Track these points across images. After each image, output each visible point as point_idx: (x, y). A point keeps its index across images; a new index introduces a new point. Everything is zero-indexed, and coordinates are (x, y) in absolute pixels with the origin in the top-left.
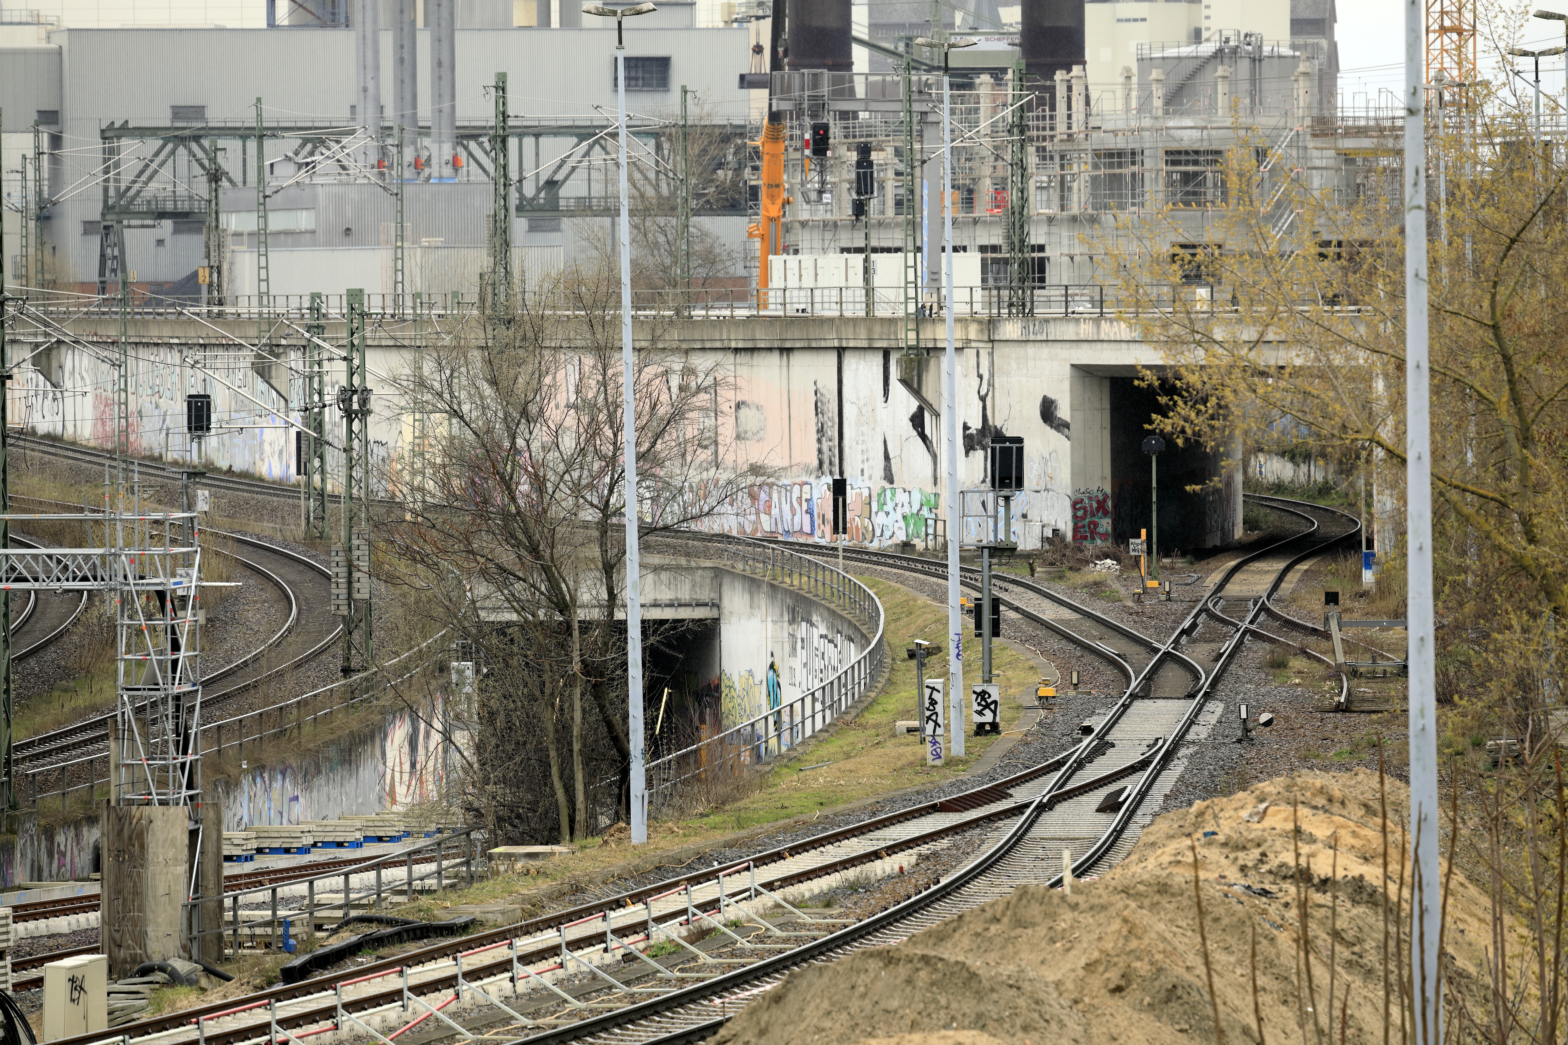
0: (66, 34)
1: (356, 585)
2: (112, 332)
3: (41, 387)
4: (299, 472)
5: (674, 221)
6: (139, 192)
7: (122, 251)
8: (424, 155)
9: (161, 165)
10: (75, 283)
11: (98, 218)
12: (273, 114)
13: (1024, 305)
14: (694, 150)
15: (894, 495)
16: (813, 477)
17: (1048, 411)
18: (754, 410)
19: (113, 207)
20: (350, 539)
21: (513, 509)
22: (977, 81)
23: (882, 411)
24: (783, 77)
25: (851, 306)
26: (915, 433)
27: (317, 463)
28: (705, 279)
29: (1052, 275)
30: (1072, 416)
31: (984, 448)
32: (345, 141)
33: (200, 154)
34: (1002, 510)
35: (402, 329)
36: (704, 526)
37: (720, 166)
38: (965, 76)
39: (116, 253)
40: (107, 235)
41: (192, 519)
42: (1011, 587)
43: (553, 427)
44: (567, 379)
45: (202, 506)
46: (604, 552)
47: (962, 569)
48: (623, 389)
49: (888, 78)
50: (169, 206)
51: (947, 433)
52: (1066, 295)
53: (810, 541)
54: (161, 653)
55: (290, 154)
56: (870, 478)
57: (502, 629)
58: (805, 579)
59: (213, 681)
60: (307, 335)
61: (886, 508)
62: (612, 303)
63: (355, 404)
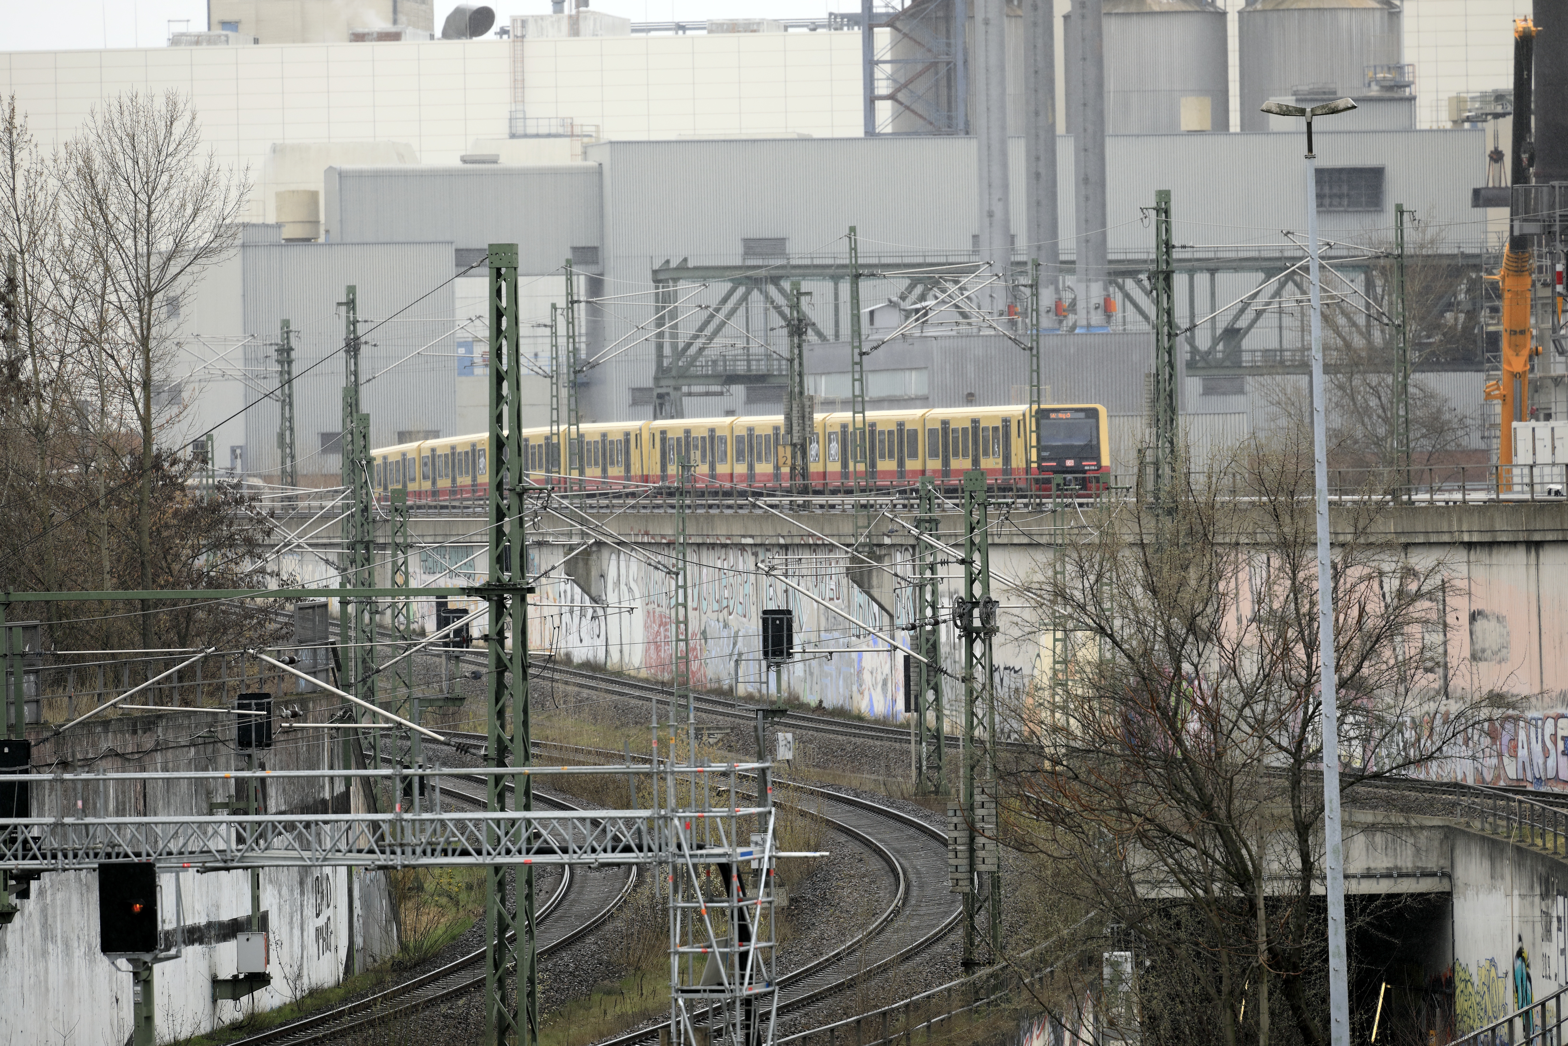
1: (981, 854)
3: (577, 602)
4: (908, 709)
5: (1390, 380)
6: (701, 350)
8: (1067, 297)
11: (650, 383)
14: (1414, 286)
18: (1493, 623)
19: (669, 369)
20: (971, 795)
21: (1179, 755)
24: (1527, 193)
27: (930, 695)
28: (1431, 454)
32: (964, 281)
33: (780, 300)
36: (1433, 772)
37: (1449, 307)
41: (763, 771)
43: (1228, 647)
45: (784, 753)
46: (1297, 808)
48: (1318, 597)
50: (741, 368)
54: (726, 944)
55: (895, 299)
57: (1165, 908)
59: (795, 980)
60: (915, 531)
62: (1301, 487)
63: (977, 619)
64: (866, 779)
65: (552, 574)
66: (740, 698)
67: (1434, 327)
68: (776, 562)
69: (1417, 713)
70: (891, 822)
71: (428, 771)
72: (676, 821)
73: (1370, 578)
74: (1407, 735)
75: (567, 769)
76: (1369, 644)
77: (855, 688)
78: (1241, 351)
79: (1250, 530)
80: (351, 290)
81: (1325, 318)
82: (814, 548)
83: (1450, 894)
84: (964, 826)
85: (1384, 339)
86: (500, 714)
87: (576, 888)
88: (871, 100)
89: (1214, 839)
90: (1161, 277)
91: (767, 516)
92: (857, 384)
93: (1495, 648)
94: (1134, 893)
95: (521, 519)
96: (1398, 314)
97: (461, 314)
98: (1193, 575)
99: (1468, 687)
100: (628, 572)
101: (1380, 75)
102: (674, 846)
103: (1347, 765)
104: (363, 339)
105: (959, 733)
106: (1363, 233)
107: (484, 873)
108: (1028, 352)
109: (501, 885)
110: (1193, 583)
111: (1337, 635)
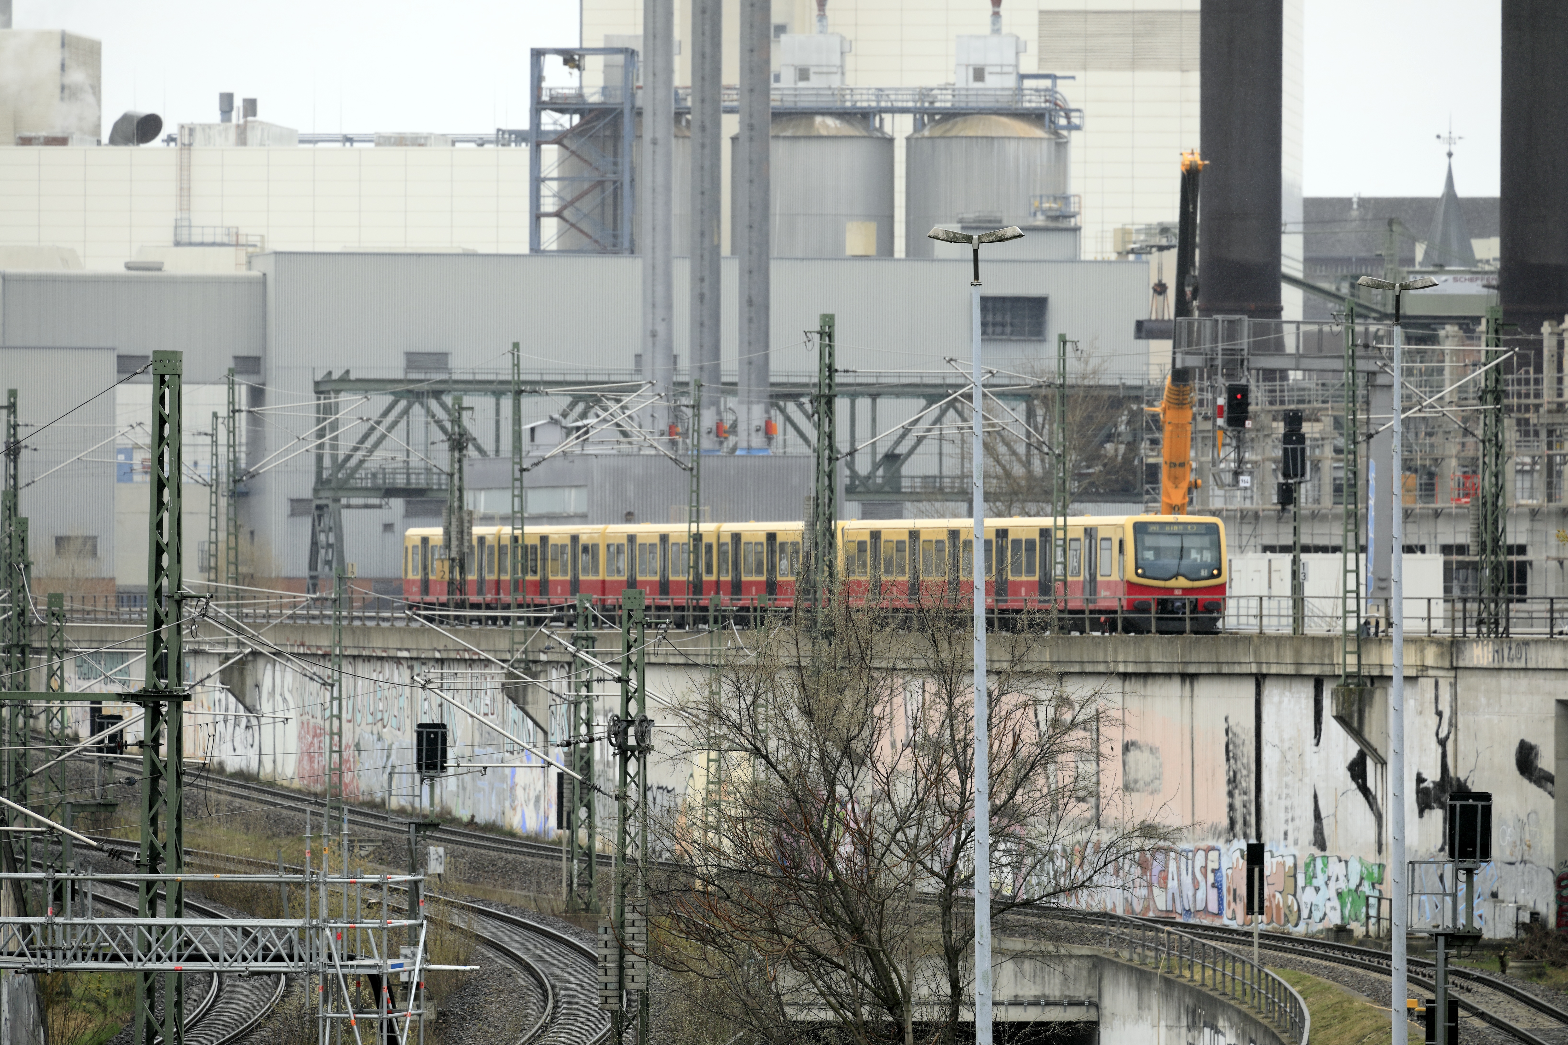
0: (272, 259)
1: (630, 972)
2: (324, 642)
3: (232, 711)
4: (560, 826)
6: (361, 462)
7: (340, 538)
8: (728, 419)
9: (390, 428)
10: (277, 578)
11: (308, 494)
12: (534, 365)
13: (1497, 623)
14: (1077, 416)
15: (1326, 865)
16: (1222, 841)
17: (1526, 759)
19: (328, 481)
20: (622, 913)
21: (831, 878)
22: (1442, 333)
23: (1313, 758)
24: (1190, 325)
25: (1274, 621)
26: (1354, 786)
27: (583, 813)
29: (1535, 585)
30: (1557, 767)
31: (1442, 806)
32: (626, 400)
33: (441, 414)
34: (1462, 886)
35: (696, 643)
36: (1083, 901)
37: (1109, 438)
38: (1427, 326)
39: (332, 540)
40: (320, 516)
41: (416, 883)
42: (1475, 986)
43: (882, 770)
44: (903, 711)
45: (436, 867)
47: (1409, 962)
48: (973, 724)
49: (1326, 328)
50: (400, 481)
51: (1397, 787)
52: (1552, 611)
53: (1217, 923)
55: (556, 416)
56: (1296, 843)
58: (1209, 973)
60: (572, 649)
61: (1316, 882)
63: (632, 738)
64: (517, 895)
65: (207, 683)
66: (393, 811)
67: (1092, 459)
68: (431, 676)
69: (1069, 841)
70: (541, 939)
71: (81, 876)
72: (328, 931)
73: (1026, 705)
74: (1058, 863)
75: (219, 877)
76: (1023, 772)
77: (507, 804)
78: (900, 477)
79: (907, 655)
80: (13, 393)
81: (985, 445)
82: (470, 662)
83: (1097, 1023)
84: (615, 944)
85: (1044, 468)
86: (154, 821)
87: (223, 997)
88: (537, 216)
89: (865, 961)
90: (823, 401)
91: (423, 630)
92: (516, 500)
93: (1148, 779)
94: (784, 1015)
95: (179, 626)
96: (1059, 444)
97: (122, 420)
98: (849, 697)
99: (1120, 816)
100: (283, 682)
101: (1046, 205)
102: (325, 956)
103: (998, 892)
104: (23, 444)
105: (612, 850)
106: (1025, 362)
107: (132, 980)
108: (688, 473)
109: (150, 991)
110: (849, 706)
111: (991, 761)
